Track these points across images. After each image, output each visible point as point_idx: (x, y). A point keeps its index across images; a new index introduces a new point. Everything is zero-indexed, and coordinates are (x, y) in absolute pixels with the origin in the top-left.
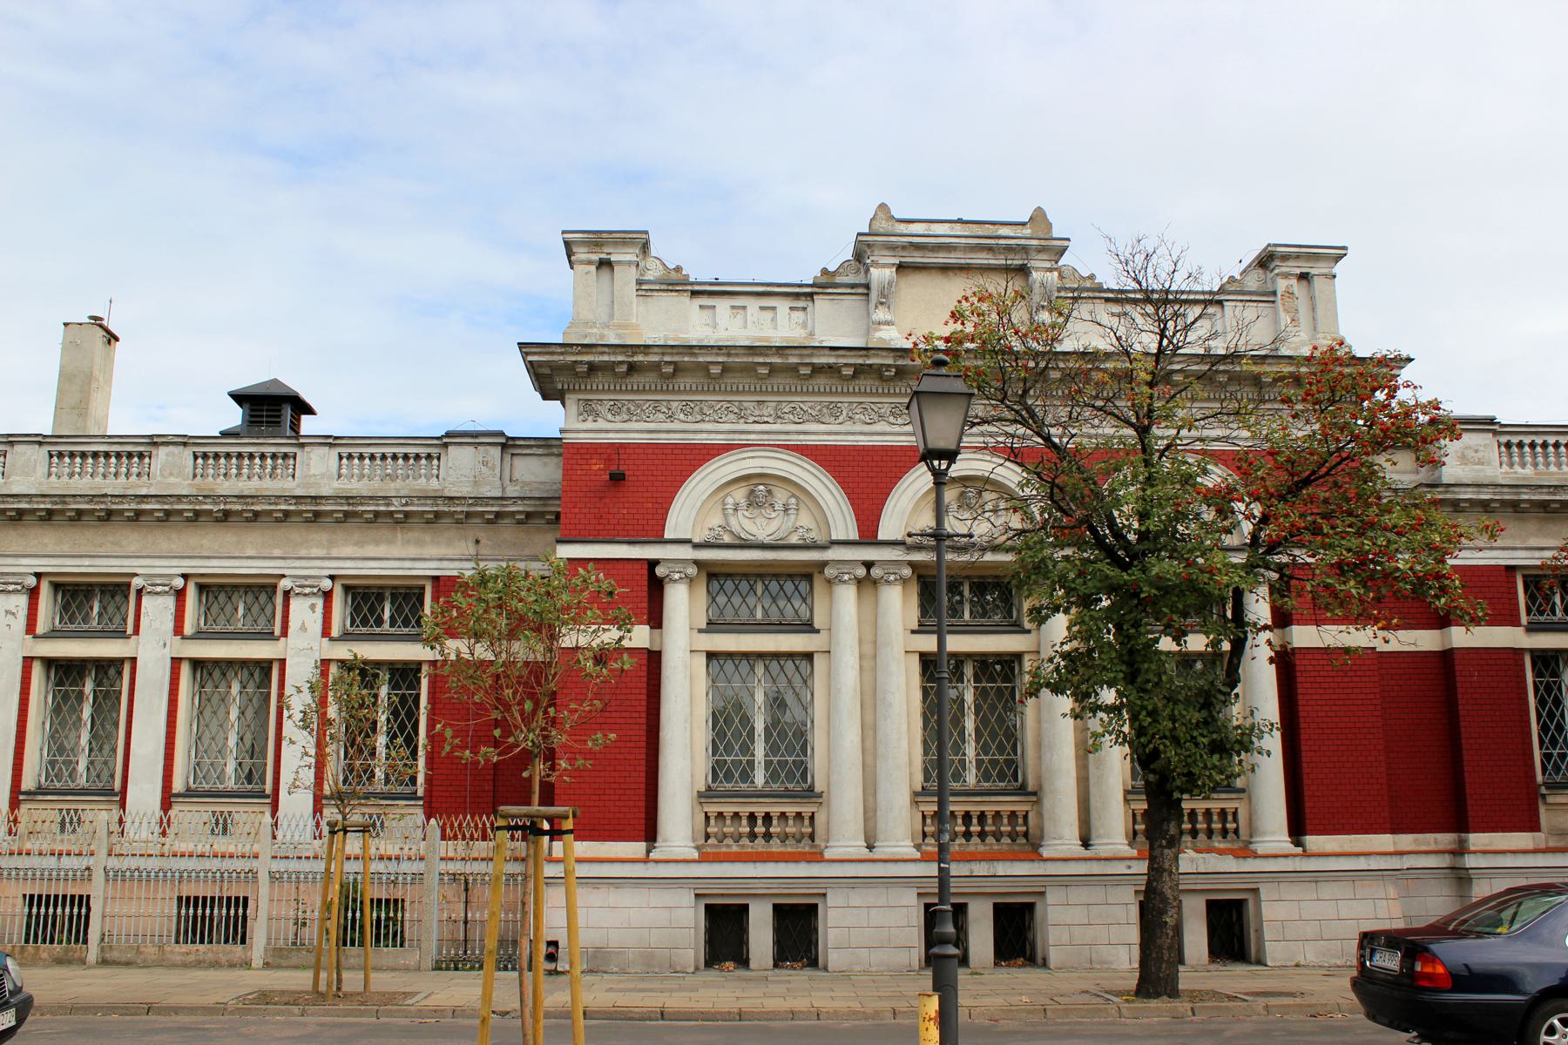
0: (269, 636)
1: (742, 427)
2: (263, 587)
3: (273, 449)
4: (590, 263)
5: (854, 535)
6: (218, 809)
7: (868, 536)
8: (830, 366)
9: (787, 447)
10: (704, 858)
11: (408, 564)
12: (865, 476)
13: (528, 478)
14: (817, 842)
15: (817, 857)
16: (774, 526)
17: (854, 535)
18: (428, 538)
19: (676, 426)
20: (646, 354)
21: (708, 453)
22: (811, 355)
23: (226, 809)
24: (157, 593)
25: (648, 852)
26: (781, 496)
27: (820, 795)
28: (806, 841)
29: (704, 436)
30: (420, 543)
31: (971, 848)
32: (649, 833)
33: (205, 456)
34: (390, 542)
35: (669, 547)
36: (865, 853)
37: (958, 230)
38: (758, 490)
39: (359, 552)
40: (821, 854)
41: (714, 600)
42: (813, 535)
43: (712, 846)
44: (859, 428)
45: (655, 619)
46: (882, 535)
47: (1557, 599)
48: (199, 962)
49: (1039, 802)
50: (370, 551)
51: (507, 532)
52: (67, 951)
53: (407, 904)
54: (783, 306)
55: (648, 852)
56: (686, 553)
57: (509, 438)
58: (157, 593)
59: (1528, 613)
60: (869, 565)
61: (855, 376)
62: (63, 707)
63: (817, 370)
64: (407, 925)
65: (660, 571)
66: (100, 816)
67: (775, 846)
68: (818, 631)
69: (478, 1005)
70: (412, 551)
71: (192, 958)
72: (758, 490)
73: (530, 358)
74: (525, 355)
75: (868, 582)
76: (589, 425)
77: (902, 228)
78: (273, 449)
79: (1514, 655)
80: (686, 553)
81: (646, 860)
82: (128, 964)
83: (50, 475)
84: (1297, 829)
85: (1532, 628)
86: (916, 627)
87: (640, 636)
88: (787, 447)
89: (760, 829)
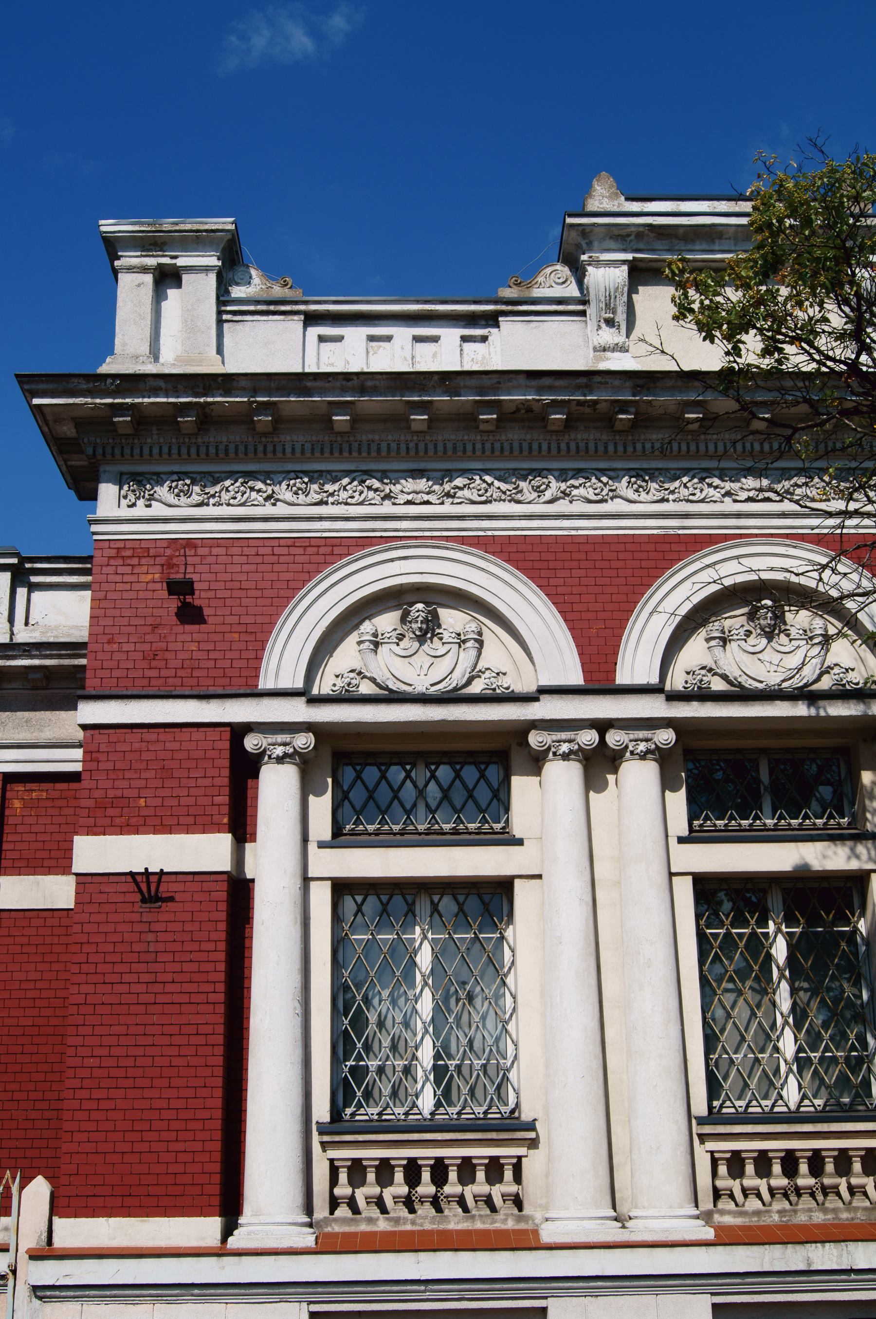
1: (387, 508)
4: (144, 270)
5: (576, 678)
7: (600, 681)
8: (526, 408)
9: (462, 540)
10: (328, 1245)
12: (594, 586)
13: (53, 620)
14: (528, 1210)
15: (525, 1241)
16: (442, 668)
17: (576, 678)
19: (281, 510)
20: (227, 393)
21: (328, 552)
22: (496, 390)
25: (228, 1231)
26: (453, 619)
27: (531, 1126)
28: (506, 1209)
29: (326, 525)
31: (802, 1218)
32: (229, 1202)
35: (266, 702)
36: (612, 1232)
38: (420, 605)
40: (536, 1232)
41: (346, 796)
42: (505, 682)
43: (343, 1221)
44: (579, 507)
45: (242, 828)
46: (623, 678)
50: (797, 1279)
55: (228, 1231)
56: (296, 711)
57: (23, 560)
60: (602, 726)
61: (569, 425)
63: (514, 416)
65: (251, 743)
67: (454, 1220)
68: (520, 842)
69: (314, 1246)
72: (420, 605)
73: (36, 401)
74: (21, 383)
75: (599, 764)
76: (140, 511)
80: (296, 711)
81: (221, 1252)
86: (685, 833)
87: (205, 852)
88: (462, 540)
89: (426, 1188)
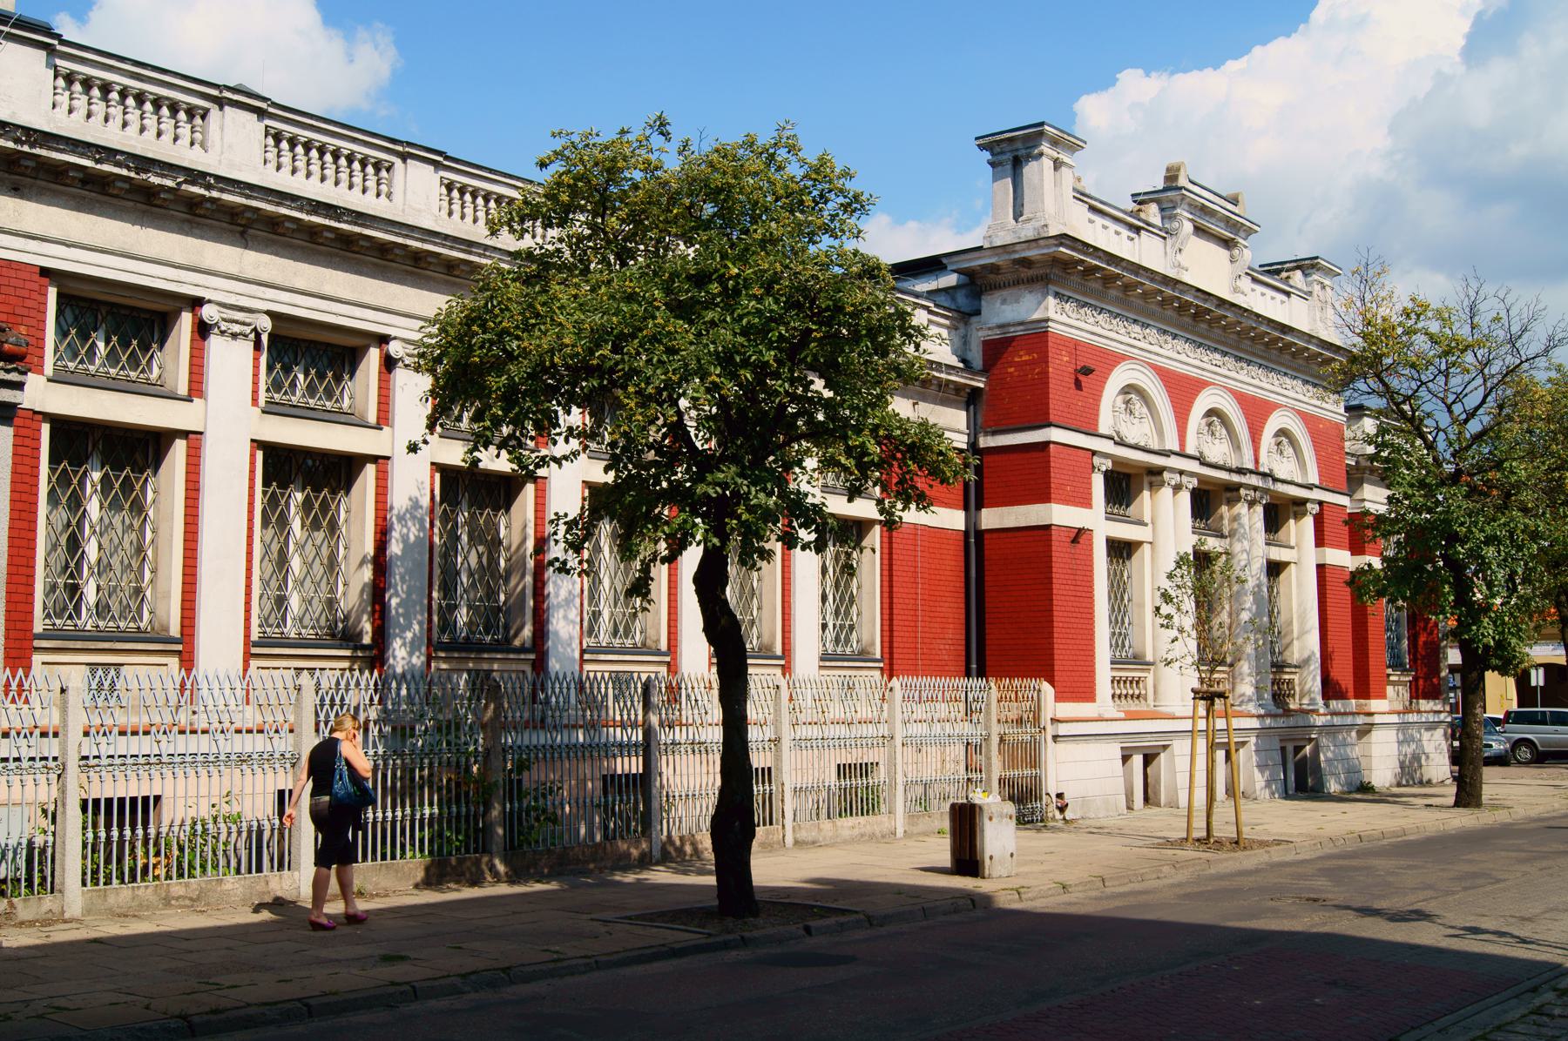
48: (862, 835)
66: (149, 676)
71: (856, 832)
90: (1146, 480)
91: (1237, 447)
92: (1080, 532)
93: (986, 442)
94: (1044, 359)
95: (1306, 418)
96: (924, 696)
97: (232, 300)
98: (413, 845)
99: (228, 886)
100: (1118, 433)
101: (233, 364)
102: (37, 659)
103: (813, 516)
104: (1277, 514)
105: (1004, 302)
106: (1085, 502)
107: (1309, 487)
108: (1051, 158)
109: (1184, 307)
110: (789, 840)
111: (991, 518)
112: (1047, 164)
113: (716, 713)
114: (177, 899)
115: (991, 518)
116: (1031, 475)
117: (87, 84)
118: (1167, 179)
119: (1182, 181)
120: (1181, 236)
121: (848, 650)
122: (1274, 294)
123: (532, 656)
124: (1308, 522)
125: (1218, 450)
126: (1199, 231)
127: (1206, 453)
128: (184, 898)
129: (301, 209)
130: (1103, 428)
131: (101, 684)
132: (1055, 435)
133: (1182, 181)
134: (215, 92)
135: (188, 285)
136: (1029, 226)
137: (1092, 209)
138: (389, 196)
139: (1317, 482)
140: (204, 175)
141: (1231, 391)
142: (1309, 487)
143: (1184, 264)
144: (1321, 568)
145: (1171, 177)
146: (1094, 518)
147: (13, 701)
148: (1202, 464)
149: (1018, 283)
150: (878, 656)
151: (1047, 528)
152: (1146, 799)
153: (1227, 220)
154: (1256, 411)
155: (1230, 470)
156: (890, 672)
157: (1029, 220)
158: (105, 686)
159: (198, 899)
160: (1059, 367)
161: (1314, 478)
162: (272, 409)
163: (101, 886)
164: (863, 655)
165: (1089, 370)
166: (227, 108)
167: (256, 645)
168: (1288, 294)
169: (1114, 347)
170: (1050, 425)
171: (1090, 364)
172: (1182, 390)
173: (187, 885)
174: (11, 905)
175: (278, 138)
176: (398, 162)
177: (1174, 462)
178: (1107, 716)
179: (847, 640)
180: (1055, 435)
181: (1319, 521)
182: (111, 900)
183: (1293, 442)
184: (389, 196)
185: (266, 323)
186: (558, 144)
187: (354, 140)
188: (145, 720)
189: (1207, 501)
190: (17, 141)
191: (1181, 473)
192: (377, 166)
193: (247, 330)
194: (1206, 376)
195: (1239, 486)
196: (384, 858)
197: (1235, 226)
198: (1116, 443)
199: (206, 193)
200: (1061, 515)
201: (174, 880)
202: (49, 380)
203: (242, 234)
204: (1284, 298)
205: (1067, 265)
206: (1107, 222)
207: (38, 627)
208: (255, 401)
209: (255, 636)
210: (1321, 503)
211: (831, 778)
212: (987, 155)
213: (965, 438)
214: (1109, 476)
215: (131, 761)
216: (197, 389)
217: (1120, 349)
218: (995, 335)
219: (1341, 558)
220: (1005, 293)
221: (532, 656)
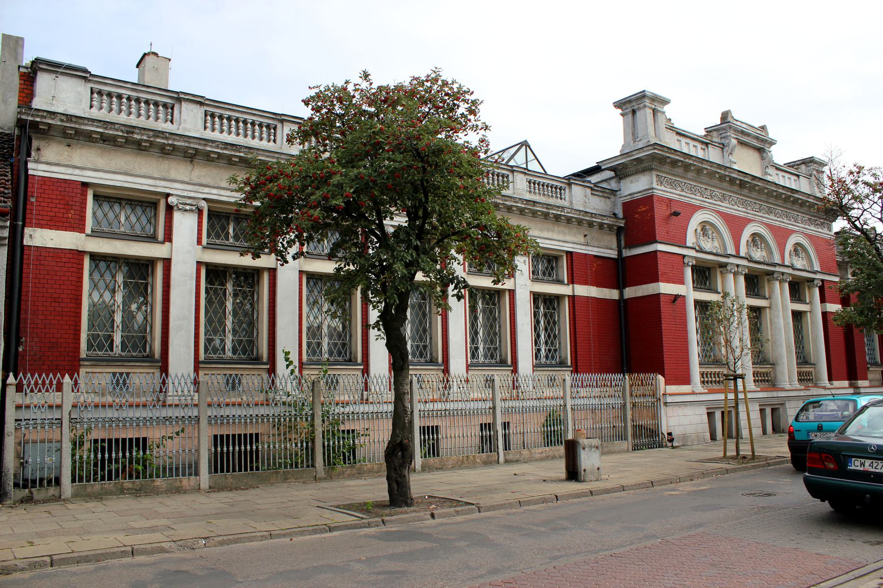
0: (152, 238)
2: (152, 203)
3: (129, 93)
6: (228, 372)
11: (561, 244)
18: (566, 231)
23: (234, 372)
24: (186, 210)
30: (564, 233)
33: (100, 93)
34: (553, 231)
37: (748, 127)
39: (561, 237)
47: (231, 231)
48: (547, 457)
49: (774, 369)
51: (594, 232)
52: (488, 457)
53: (511, 425)
54: (699, 146)
58: (186, 210)
59: (208, 236)
62: (215, 299)
64: (511, 436)
66: (142, 378)
70: (561, 237)
71: (544, 455)
77: (735, 122)
78: (129, 93)
79: (78, 255)
82: (517, 461)
83: (91, 107)
84: (830, 379)
85: (96, 234)
90: (718, 270)
91: (770, 252)
92: (676, 298)
93: (627, 253)
94: (652, 209)
95: (810, 237)
96: (613, 384)
97: (185, 194)
98: (268, 459)
99: (158, 484)
100: (699, 246)
101: (185, 225)
102: (82, 371)
103: (461, 284)
104: (797, 288)
105: (631, 182)
106: (681, 281)
107: (815, 272)
108: (651, 108)
109: (732, 181)
110: (502, 459)
111: (631, 292)
112: (649, 112)
113: (391, 396)
114: (128, 489)
115: (631, 292)
116: (648, 268)
117: (110, 95)
118: (722, 119)
119: (729, 119)
120: (731, 146)
121: (554, 362)
122: (790, 176)
123: (268, 367)
124: (817, 291)
125: (758, 255)
126: (741, 143)
127: (753, 255)
128: (132, 489)
129: (217, 147)
130: (689, 244)
131: (118, 381)
132: (661, 247)
133: (729, 119)
134: (176, 96)
135: (161, 187)
136: (640, 143)
137: (678, 134)
138: (274, 141)
139: (819, 270)
140: (163, 132)
141: (765, 224)
142: (815, 272)
143: (733, 160)
144: (825, 314)
145: (725, 116)
146: (687, 290)
147: (47, 391)
148: (749, 261)
149: (637, 172)
150: (569, 364)
151: (658, 295)
152: (774, 429)
153: (757, 138)
154: (782, 235)
155: (768, 265)
156: (576, 370)
157: (641, 140)
158: (121, 383)
159: (140, 490)
160: (660, 212)
161: (817, 267)
162: (210, 247)
163: (84, 483)
164: (562, 364)
165: (679, 213)
166: (183, 103)
167: (203, 363)
168: (798, 176)
169: (693, 202)
170: (656, 242)
171: (678, 210)
172: (736, 225)
173: (133, 483)
174: (31, 492)
175: (213, 116)
176: (279, 126)
177: (732, 260)
178: (697, 391)
179: (553, 357)
180: (661, 247)
181: (822, 289)
182: (89, 489)
183: (804, 249)
184: (274, 141)
185: (204, 205)
186: (312, 93)
187: (254, 115)
188: (144, 399)
189: (755, 282)
190: (62, 121)
191: (738, 266)
192: (268, 127)
193: (194, 208)
194: (750, 216)
195: (773, 273)
196: (252, 469)
197: (764, 141)
198: (697, 251)
199: (165, 141)
200: (666, 288)
201: (84, 483)
202: (204, 248)
203: (191, 162)
204: (796, 178)
205: (662, 160)
206: (688, 141)
207: (83, 355)
208: (199, 242)
209: (202, 357)
210: (822, 281)
211: (478, 432)
212: (620, 111)
213: (616, 253)
214: (694, 269)
215: (32, 422)
216: (168, 238)
217: (697, 203)
218: (628, 199)
219: (834, 307)
220: (631, 178)
221: (268, 367)
